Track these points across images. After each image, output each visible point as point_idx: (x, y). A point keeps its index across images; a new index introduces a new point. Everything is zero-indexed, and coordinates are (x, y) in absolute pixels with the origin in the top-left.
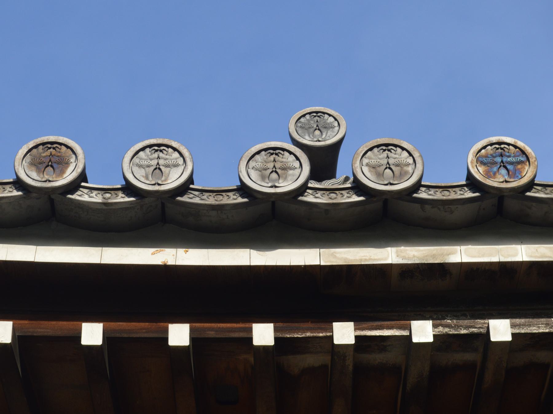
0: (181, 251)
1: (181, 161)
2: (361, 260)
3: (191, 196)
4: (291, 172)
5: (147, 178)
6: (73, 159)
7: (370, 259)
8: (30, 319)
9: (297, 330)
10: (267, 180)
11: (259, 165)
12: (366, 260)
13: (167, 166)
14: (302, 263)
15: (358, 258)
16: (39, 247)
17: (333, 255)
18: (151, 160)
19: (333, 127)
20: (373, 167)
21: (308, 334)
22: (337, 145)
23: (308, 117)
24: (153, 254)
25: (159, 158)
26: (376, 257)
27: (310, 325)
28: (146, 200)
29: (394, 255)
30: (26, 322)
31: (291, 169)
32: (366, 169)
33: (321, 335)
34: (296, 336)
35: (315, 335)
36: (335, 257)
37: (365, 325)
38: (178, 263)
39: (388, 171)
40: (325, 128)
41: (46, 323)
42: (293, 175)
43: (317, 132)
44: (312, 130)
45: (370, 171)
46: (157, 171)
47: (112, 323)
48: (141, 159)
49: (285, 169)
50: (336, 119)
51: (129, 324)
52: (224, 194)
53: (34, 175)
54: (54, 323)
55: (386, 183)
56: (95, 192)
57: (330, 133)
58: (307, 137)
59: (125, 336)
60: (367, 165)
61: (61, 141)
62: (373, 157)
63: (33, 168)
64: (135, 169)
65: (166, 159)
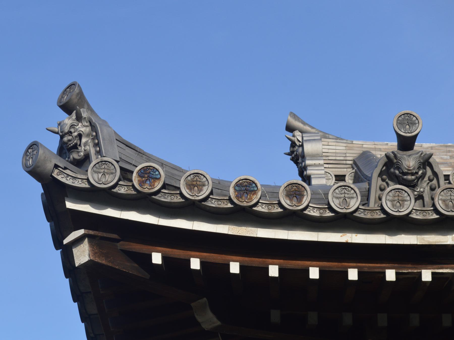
0: (354, 235)
1: (355, 195)
2: (436, 242)
3: (360, 212)
4: (406, 203)
5: (340, 205)
6: (305, 193)
7: (440, 242)
8: (284, 260)
9: (405, 268)
10: (395, 207)
11: (391, 198)
12: (438, 242)
13: (349, 198)
14: (409, 243)
15: (434, 241)
16: (289, 232)
17: (423, 239)
18: (341, 194)
19: (415, 124)
20: (444, 201)
21: (410, 271)
22: (417, 135)
23: (403, 116)
24: (341, 236)
25: (345, 193)
26: (443, 241)
27: (410, 266)
28: (339, 215)
29: (451, 240)
30: (282, 261)
31: (406, 201)
32: (440, 202)
33: (415, 271)
34: (404, 271)
35: (413, 271)
36: (424, 240)
37: (435, 266)
38: (353, 242)
39: (450, 203)
40: (412, 124)
41: (291, 261)
42: (407, 205)
43: (407, 127)
44: (405, 125)
45: (442, 203)
46: (344, 200)
47: (321, 263)
48: (337, 194)
49: (404, 201)
50: (417, 119)
51: (328, 263)
52: (374, 211)
53: (288, 202)
54: (294, 262)
55: (450, 210)
56: (316, 209)
57: (414, 128)
58: (402, 130)
59: (327, 269)
60: (441, 200)
61: (299, 183)
62: (444, 195)
63: (288, 198)
64: (334, 199)
65: (348, 194)
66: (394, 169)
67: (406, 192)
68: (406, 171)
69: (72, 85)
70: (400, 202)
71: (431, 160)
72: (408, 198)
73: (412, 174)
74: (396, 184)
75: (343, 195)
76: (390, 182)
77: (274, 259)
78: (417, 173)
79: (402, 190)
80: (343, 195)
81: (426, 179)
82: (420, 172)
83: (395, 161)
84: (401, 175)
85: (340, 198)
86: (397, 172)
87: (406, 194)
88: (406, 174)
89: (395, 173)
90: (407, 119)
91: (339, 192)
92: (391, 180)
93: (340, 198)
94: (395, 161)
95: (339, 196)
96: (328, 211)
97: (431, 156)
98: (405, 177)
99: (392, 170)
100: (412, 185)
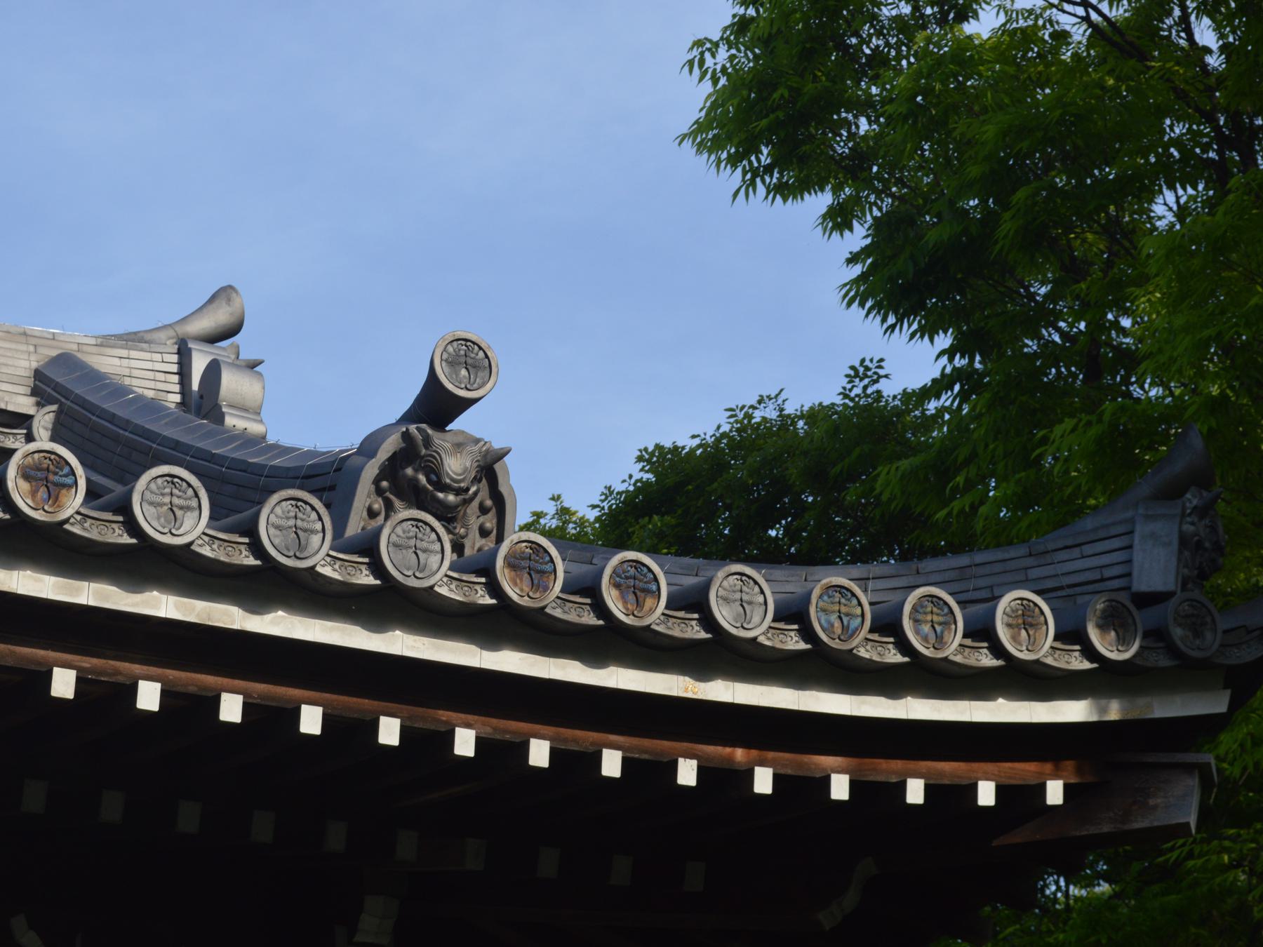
13: (181, 508)
22: (475, 401)
43: (464, 372)
48: (152, 492)
64: (145, 506)
66: (416, 470)
67: (306, 503)
68: (448, 481)
69: (224, 293)
70: (300, 532)
71: (497, 467)
72: (437, 547)
73: (458, 492)
74: (409, 507)
75: (167, 500)
76: (397, 503)
77: (195, 672)
78: (468, 489)
79: (426, 523)
80: (167, 500)
81: (475, 503)
82: (473, 489)
83: (423, 451)
84: (430, 488)
85: (161, 505)
86: (422, 479)
87: (314, 516)
88: (445, 488)
89: (417, 480)
90: (471, 356)
91: (404, 532)
92: (400, 496)
93: (161, 505)
94: (423, 451)
95: (158, 499)
96: (365, 572)
97: (501, 455)
98: (441, 495)
99: (409, 471)
100: (447, 516)
